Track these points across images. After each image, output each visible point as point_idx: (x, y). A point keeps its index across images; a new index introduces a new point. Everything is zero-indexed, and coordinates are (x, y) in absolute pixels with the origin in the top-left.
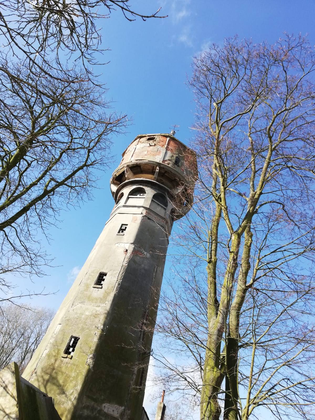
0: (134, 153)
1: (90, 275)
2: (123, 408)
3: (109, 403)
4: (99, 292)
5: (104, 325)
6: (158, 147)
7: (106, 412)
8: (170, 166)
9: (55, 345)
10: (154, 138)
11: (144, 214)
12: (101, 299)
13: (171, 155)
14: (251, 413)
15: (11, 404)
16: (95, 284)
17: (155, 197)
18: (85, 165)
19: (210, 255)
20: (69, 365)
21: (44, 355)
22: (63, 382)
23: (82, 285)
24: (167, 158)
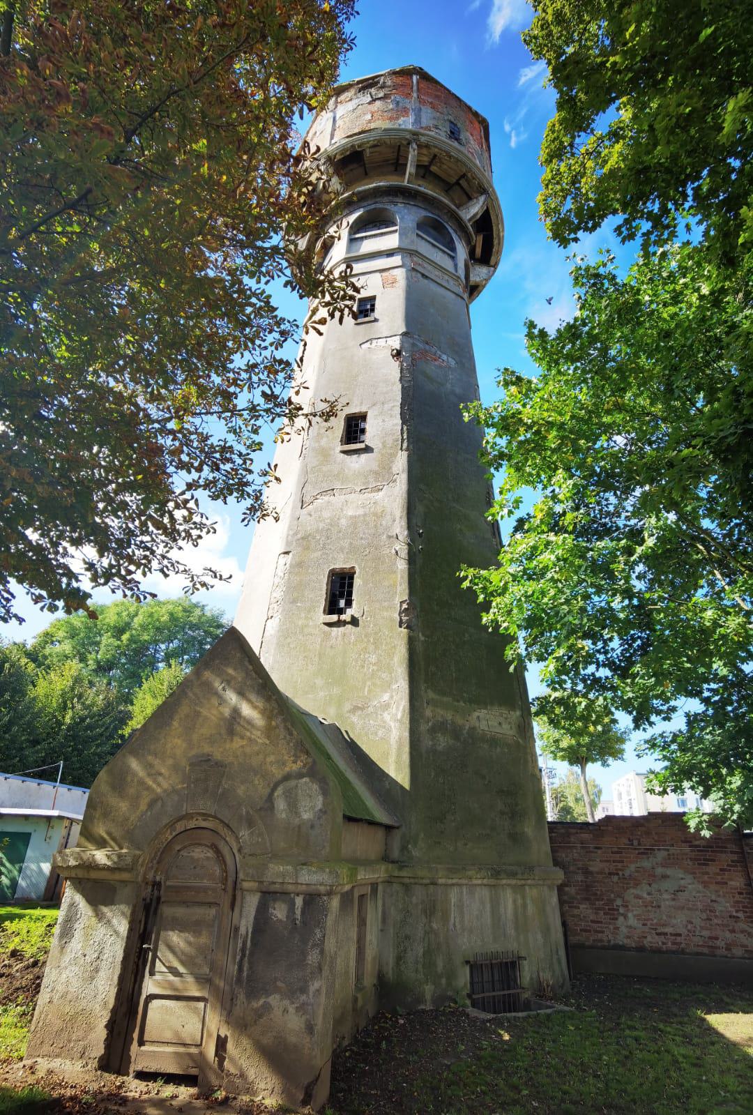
12: (376, 473)
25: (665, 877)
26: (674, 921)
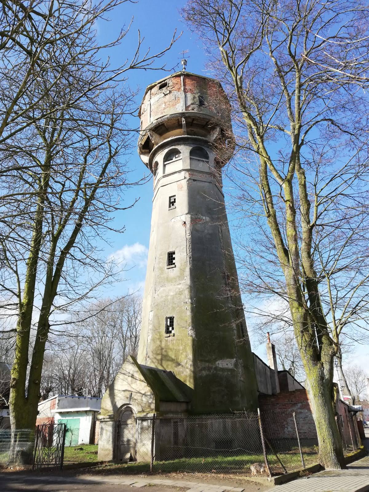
0: (151, 111)
1: (159, 259)
2: (235, 359)
3: (221, 360)
4: (174, 272)
5: (191, 298)
6: (175, 93)
7: (221, 367)
8: (195, 111)
9: (155, 330)
10: (166, 83)
11: (188, 177)
12: (179, 277)
13: (192, 97)
14: (340, 333)
15: (143, 386)
16: (168, 266)
17: (192, 153)
18: (111, 157)
19: (267, 208)
20: (174, 342)
21: (149, 341)
22: (175, 356)
23: (156, 270)
24: (189, 103)
25: (301, 413)
26: (304, 428)
